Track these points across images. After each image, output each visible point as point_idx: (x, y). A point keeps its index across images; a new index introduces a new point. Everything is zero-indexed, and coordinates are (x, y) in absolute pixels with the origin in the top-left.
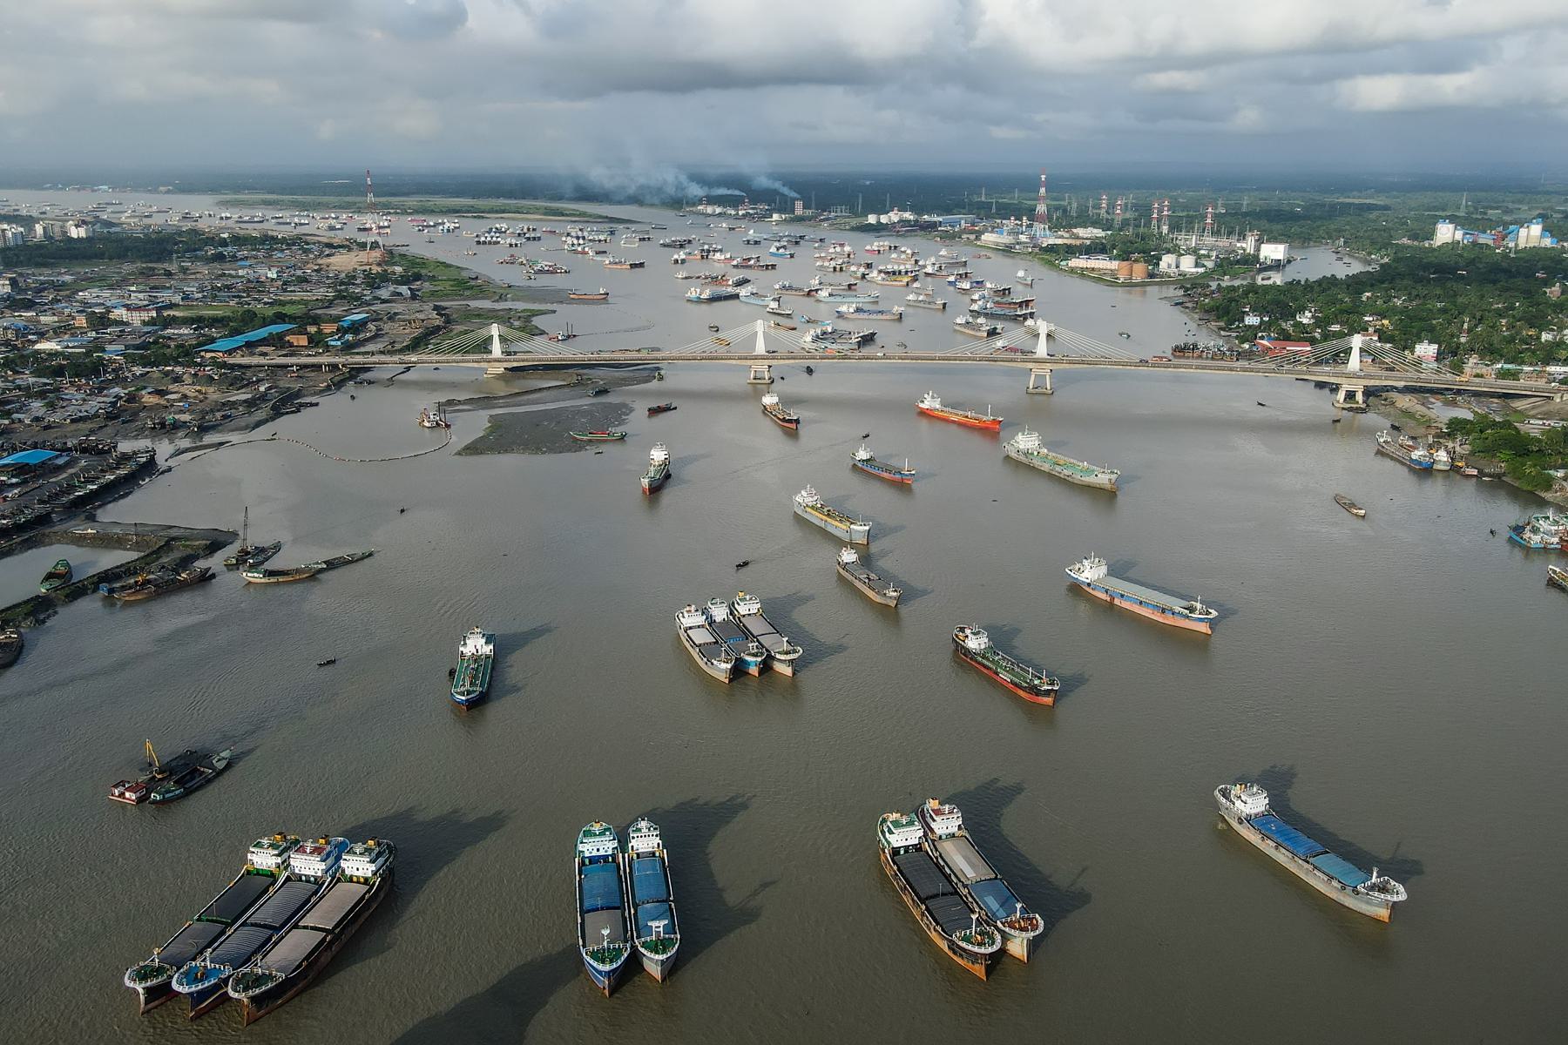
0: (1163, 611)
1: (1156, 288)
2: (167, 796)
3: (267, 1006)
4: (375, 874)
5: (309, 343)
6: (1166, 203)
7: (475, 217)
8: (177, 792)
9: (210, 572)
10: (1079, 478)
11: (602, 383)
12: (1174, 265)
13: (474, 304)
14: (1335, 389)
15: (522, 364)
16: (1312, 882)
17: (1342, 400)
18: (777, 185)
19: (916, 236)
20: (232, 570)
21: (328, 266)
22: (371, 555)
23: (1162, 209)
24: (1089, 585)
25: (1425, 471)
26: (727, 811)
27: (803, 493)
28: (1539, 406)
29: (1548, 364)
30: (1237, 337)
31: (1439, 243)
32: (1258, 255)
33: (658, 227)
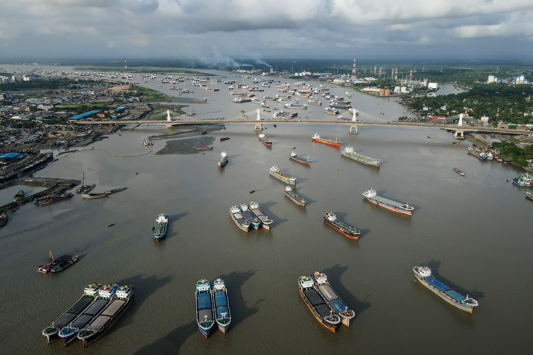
0: (395, 207)
2: (57, 270)
3: (91, 342)
4: (127, 297)
5: (105, 117)
6: (396, 69)
7: (161, 74)
8: (60, 269)
9: (71, 195)
10: (367, 162)
11: (205, 130)
12: (399, 90)
14: (454, 132)
15: (177, 124)
17: (456, 136)
19: (311, 80)
20: (79, 194)
21: (111, 90)
22: (126, 188)
23: (395, 71)
24: (370, 199)
25: (484, 160)
27: (273, 167)
28: (523, 138)
29: (526, 124)
30: (420, 115)
31: (489, 83)
32: (428, 87)
33: (224, 77)
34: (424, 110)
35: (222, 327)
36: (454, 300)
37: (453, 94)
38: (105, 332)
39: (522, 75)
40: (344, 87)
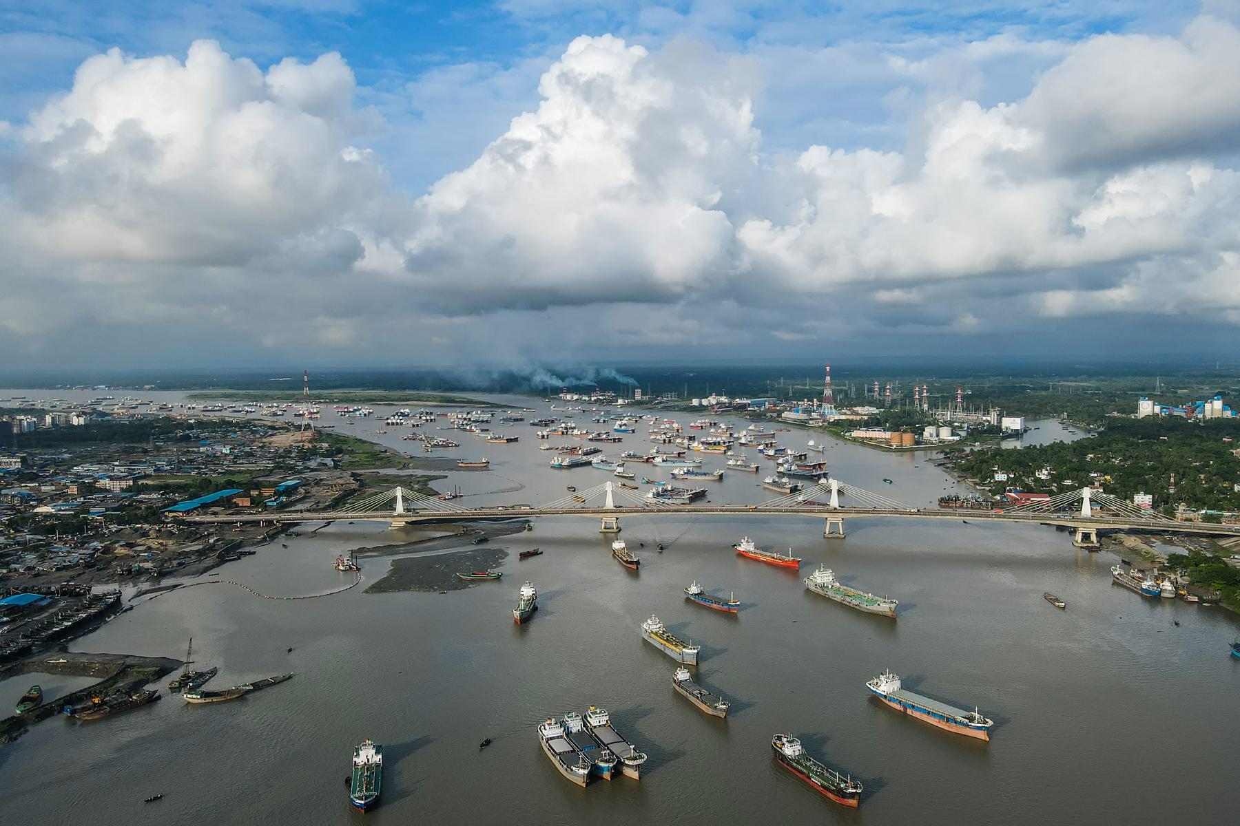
0: (948, 720)
1: (922, 453)
5: (251, 504)
6: (925, 387)
7: (386, 404)
9: (157, 695)
10: (865, 606)
12: (934, 435)
13: (383, 471)
14: (1073, 531)
17: (1080, 541)
19: (730, 415)
21: (270, 444)
22: (290, 677)
23: (921, 391)
24: (885, 697)
25: (1154, 598)
31: (1142, 416)
32: (1001, 426)
34: (997, 479)
39: (1216, 398)
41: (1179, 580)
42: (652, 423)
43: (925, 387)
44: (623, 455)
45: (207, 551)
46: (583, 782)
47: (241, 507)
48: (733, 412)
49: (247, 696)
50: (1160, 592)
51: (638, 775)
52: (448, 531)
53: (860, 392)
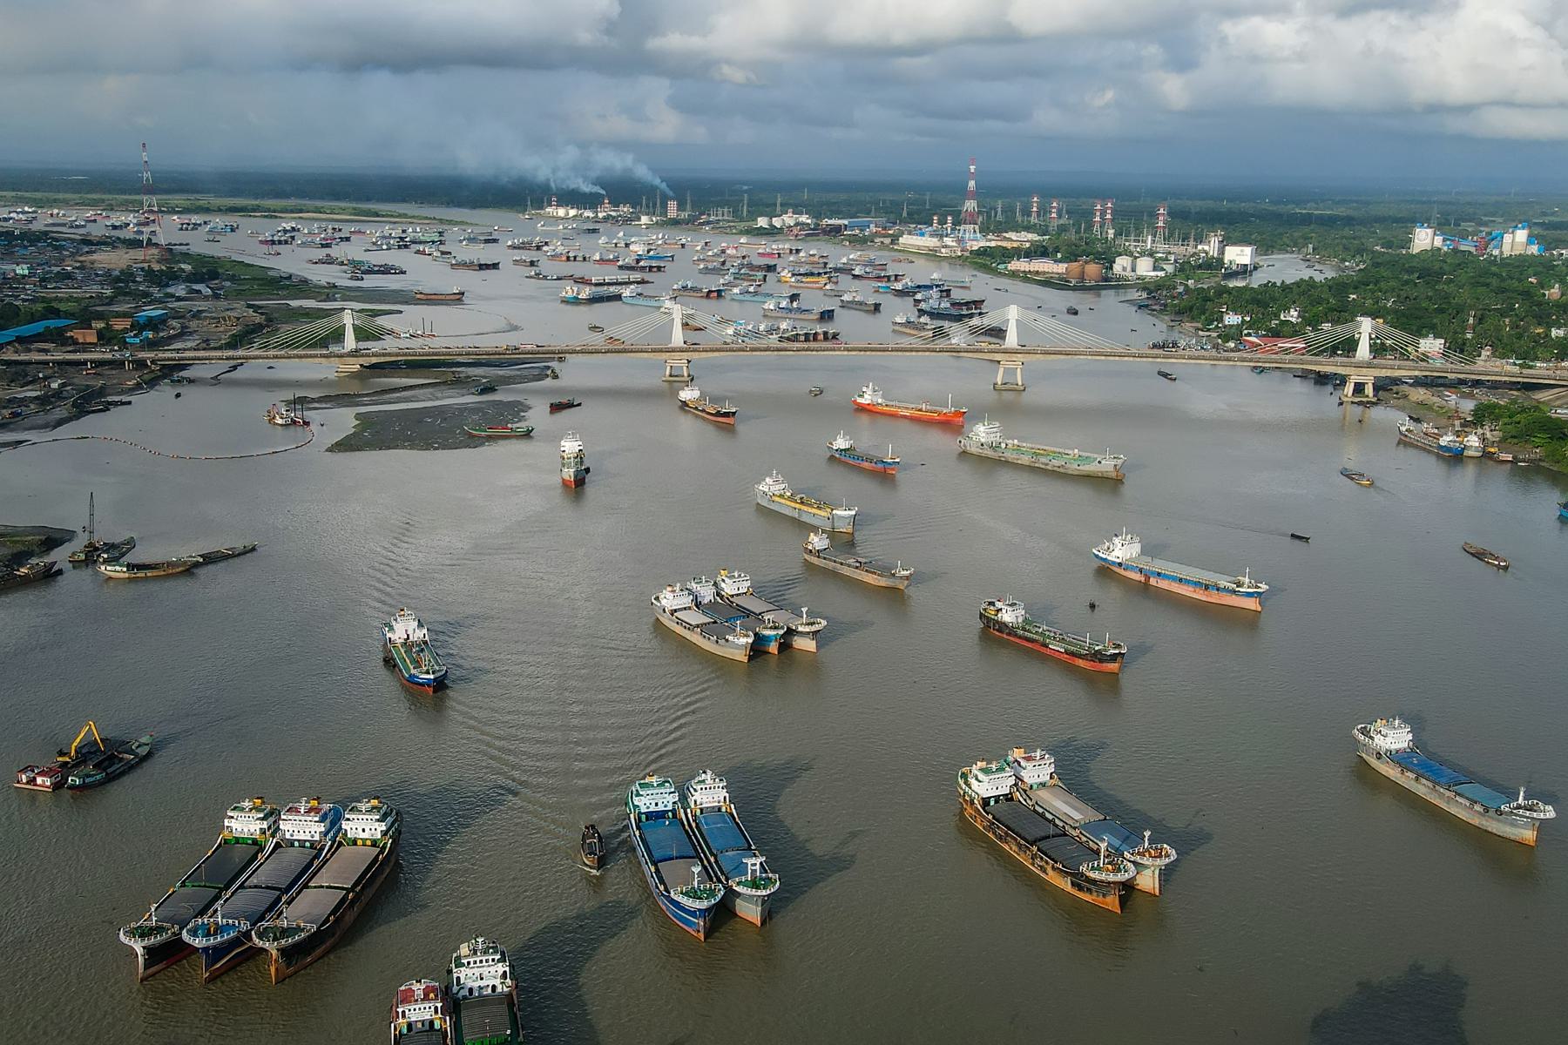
0: (1207, 587)
1: (1112, 292)
2: (87, 780)
3: (296, 964)
4: (385, 834)
5: (99, 340)
6: (1109, 205)
7: (265, 217)
8: (98, 777)
9: (55, 568)
10: (1073, 468)
12: (1129, 269)
13: (294, 303)
14: (1343, 380)
15: (382, 359)
16: (1454, 810)
18: (657, 181)
19: (818, 240)
20: (80, 567)
21: (93, 264)
22: (254, 549)
23: (1103, 211)
24: (1120, 564)
25: (1456, 457)
26: (791, 772)
27: (768, 480)
28: (1563, 396)
29: (1562, 360)
30: (1219, 337)
31: (1415, 250)
32: (1222, 259)
34: (1227, 323)
35: (750, 912)
36: (1478, 808)
37: (1311, 278)
38: (336, 936)
40: (939, 261)
41: (1488, 435)
42: (699, 248)
43: (1109, 205)
44: (675, 287)
45: (53, 399)
46: (745, 655)
47: (82, 343)
48: (821, 237)
49: (195, 571)
50: (1463, 449)
51: (815, 646)
52: (428, 378)
53: (1009, 211)
